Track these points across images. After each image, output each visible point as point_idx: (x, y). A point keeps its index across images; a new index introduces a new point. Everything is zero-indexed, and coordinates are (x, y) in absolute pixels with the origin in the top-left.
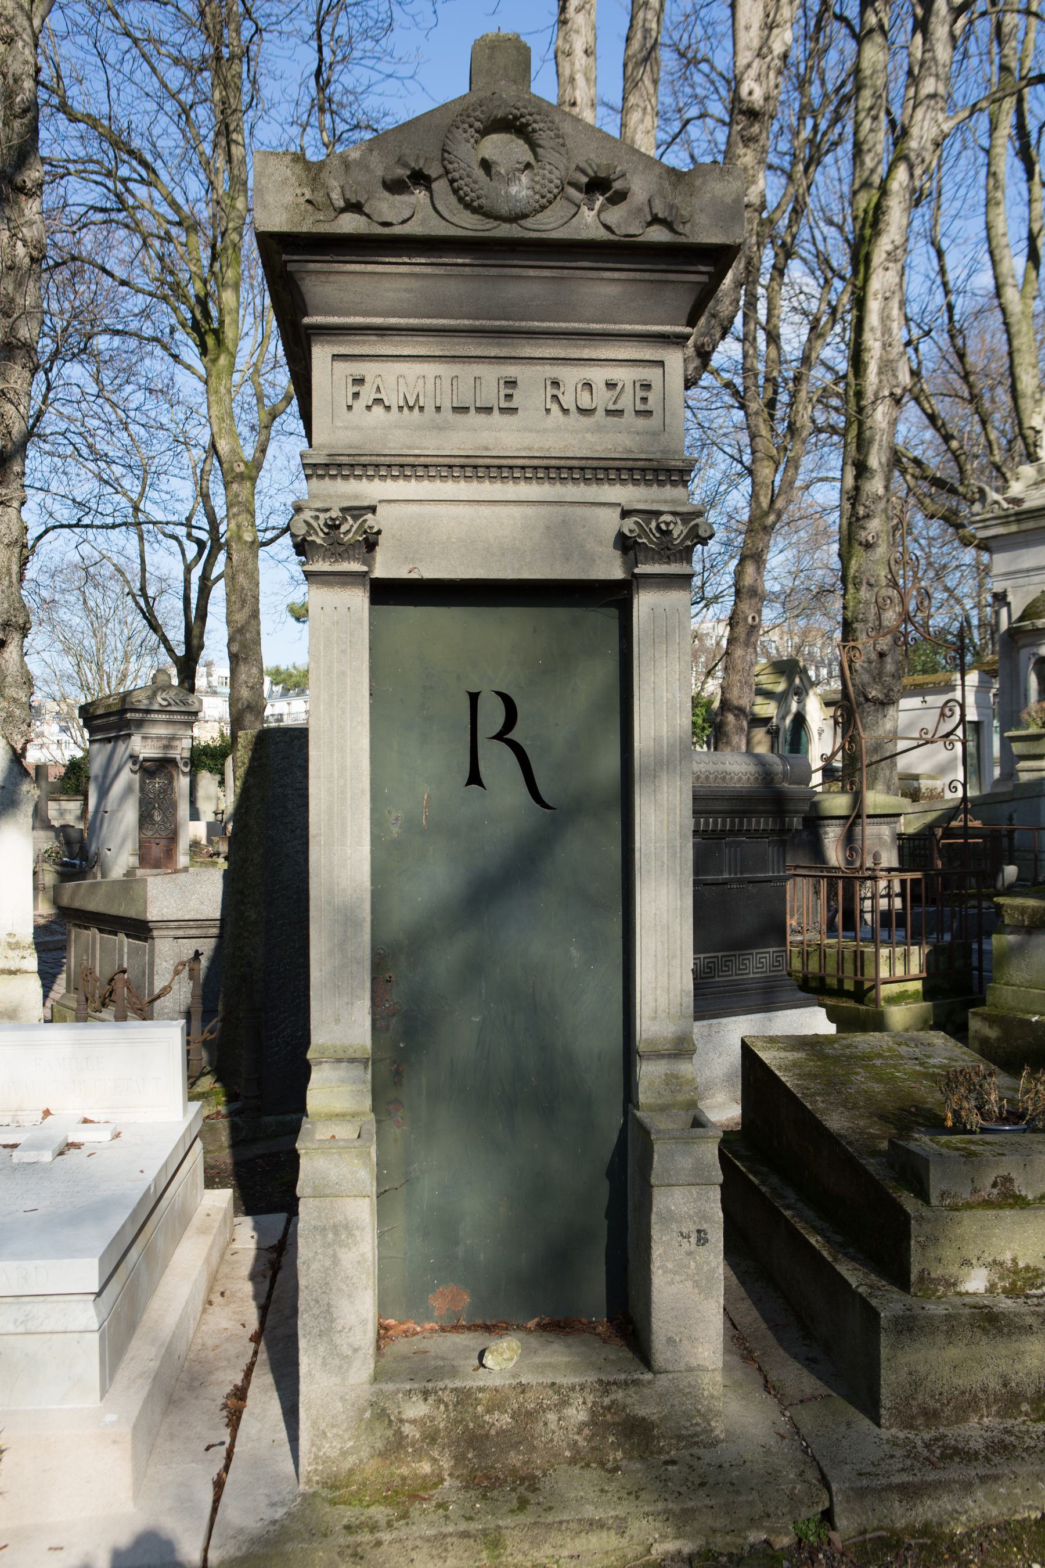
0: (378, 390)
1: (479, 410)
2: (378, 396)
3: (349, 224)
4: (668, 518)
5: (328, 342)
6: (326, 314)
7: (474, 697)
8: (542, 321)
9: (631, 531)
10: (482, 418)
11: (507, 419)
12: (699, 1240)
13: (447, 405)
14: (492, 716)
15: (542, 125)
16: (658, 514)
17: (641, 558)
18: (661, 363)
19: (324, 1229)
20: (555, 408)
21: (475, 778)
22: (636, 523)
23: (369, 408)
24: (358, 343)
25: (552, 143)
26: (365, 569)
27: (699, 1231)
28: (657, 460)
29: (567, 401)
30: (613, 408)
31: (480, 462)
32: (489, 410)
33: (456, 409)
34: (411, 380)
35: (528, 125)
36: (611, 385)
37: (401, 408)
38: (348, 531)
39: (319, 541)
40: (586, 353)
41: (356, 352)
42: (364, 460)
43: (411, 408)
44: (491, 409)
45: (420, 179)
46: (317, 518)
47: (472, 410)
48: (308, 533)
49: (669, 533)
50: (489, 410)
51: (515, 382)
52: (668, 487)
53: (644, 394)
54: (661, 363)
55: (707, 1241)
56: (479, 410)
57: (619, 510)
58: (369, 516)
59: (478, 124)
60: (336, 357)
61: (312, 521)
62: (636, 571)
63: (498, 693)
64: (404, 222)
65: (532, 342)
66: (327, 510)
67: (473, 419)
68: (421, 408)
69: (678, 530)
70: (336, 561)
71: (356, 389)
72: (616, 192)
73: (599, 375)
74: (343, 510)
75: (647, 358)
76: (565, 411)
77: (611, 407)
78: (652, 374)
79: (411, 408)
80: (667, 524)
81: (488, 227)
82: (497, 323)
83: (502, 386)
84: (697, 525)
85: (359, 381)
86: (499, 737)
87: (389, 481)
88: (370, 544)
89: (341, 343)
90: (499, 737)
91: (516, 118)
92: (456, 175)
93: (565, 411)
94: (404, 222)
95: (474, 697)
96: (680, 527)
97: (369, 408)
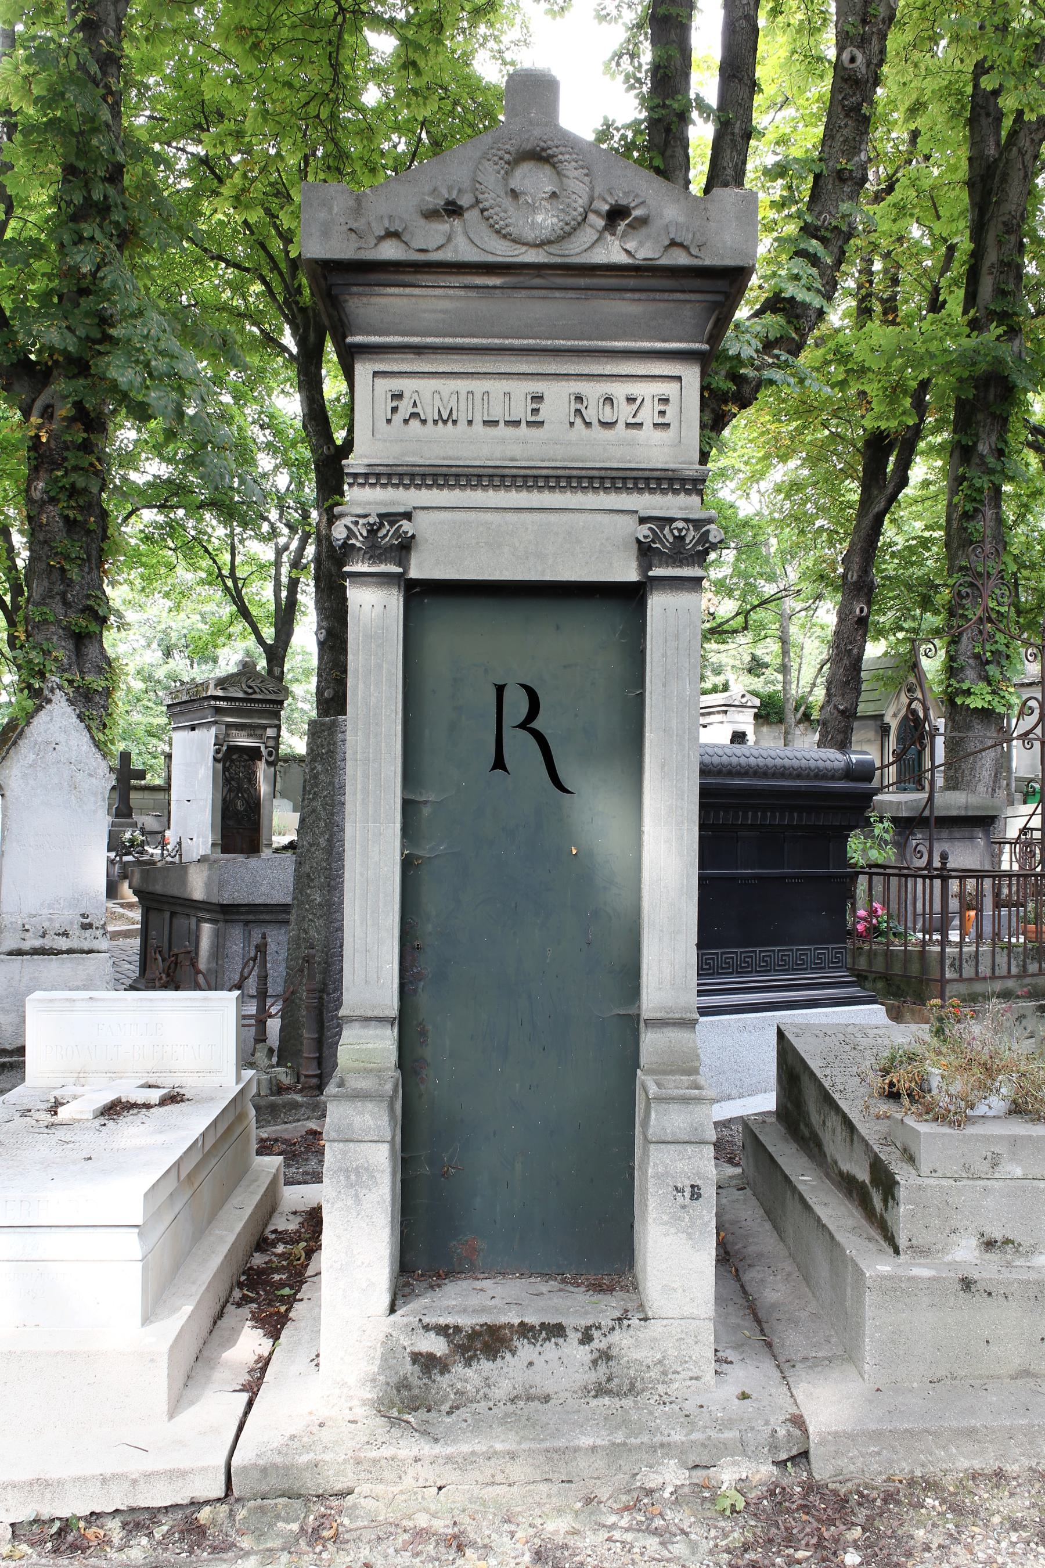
0: (415, 405)
1: (508, 423)
2: (415, 410)
3: (390, 251)
4: (680, 524)
5: (370, 360)
6: (368, 334)
7: (500, 689)
8: (568, 339)
9: (645, 537)
10: (511, 431)
11: (534, 432)
12: (692, 1195)
13: (478, 420)
14: (517, 706)
15: (567, 157)
16: (671, 520)
17: (655, 562)
18: (679, 378)
19: (347, 1170)
20: (578, 421)
21: (499, 763)
22: (650, 529)
23: (406, 421)
24: (396, 360)
25: (576, 173)
26: (401, 570)
27: (692, 1186)
28: (673, 471)
29: (590, 415)
30: (633, 421)
31: (507, 472)
32: (517, 423)
33: (486, 423)
34: (445, 394)
35: (553, 156)
36: (631, 400)
37: (435, 422)
38: (386, 536)
39: (358, 545)
40: (586, 369)
41: (396, 369)
42: (400, 470)
43: (445, 422)
44: (519, 422)
45: (453, 210)
46: (356, 523)
47: (502, 424)
48: (348, 538)
49: (681, 538)
50: (517, 423)
51: (542, 398)
52: (682, 495)
53: (662, 408)
54: (679, 378)
55: (700, 1196)
56: (508, 423)
57: (636, 517)
58: (404, 522)
59: (507, 157)
60: (376, 374)
61: (352, 526)
62: (651, 573)
63: (522, 685)
64: (438, 248)
65: (558, 359)
66: (366, 516)
67: (502, 430)
68: (455, 422)
69: (691, 535)
70: (374, 563)
71: (395, 404)
72: (636, 219)
73: (620, 390)
74: (380, 516)
75: (666, 373)
76: (588, 425)
77: (631, 421)
78: (669, 389)
79: (445, 422)
80: (680, 530)
81: (516, 253)
82: (525, 342)
83: (529, 400)
84: (708, 531)
85: (398, 396)
86: (523, 726)
87: (682, 495)
88: (405, 547)
89: (381, 361)
90: (523, 726)
91: (543, 149)
92: (487, 204)
93: (588, 425)
94: (438, 248)
95: (500, 689)
96: (692, 533)
97: (406, 421)
